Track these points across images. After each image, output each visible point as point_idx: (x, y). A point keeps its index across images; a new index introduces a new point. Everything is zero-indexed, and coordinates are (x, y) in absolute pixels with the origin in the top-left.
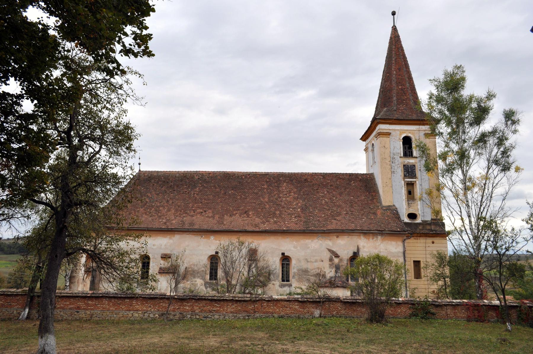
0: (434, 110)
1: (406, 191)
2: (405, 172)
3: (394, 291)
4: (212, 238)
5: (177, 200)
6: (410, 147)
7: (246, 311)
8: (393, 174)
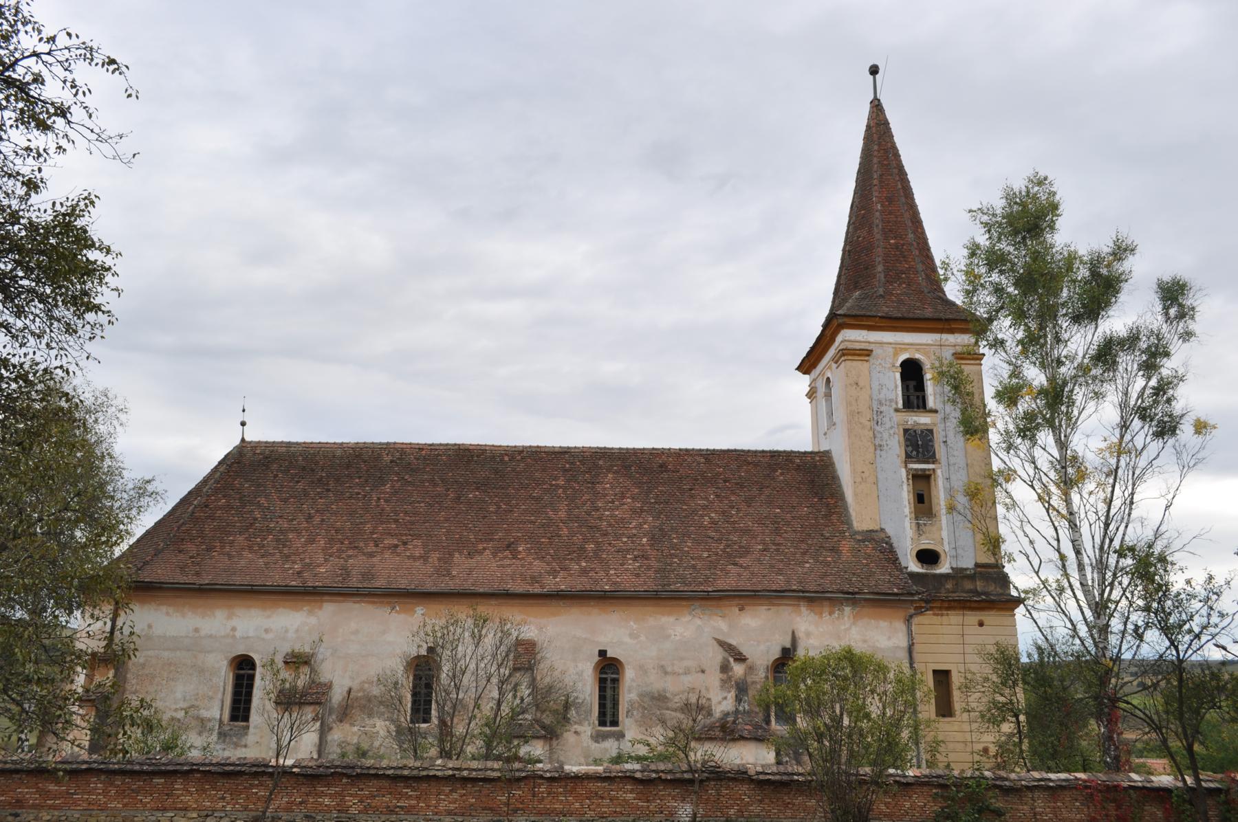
0: (982, 285)
1: (911, 496)
2: (907, 446)
3: (891, 750)
5: (335, 514)
6: (920, 387)
7: (491, 809)
8: (878, 452)
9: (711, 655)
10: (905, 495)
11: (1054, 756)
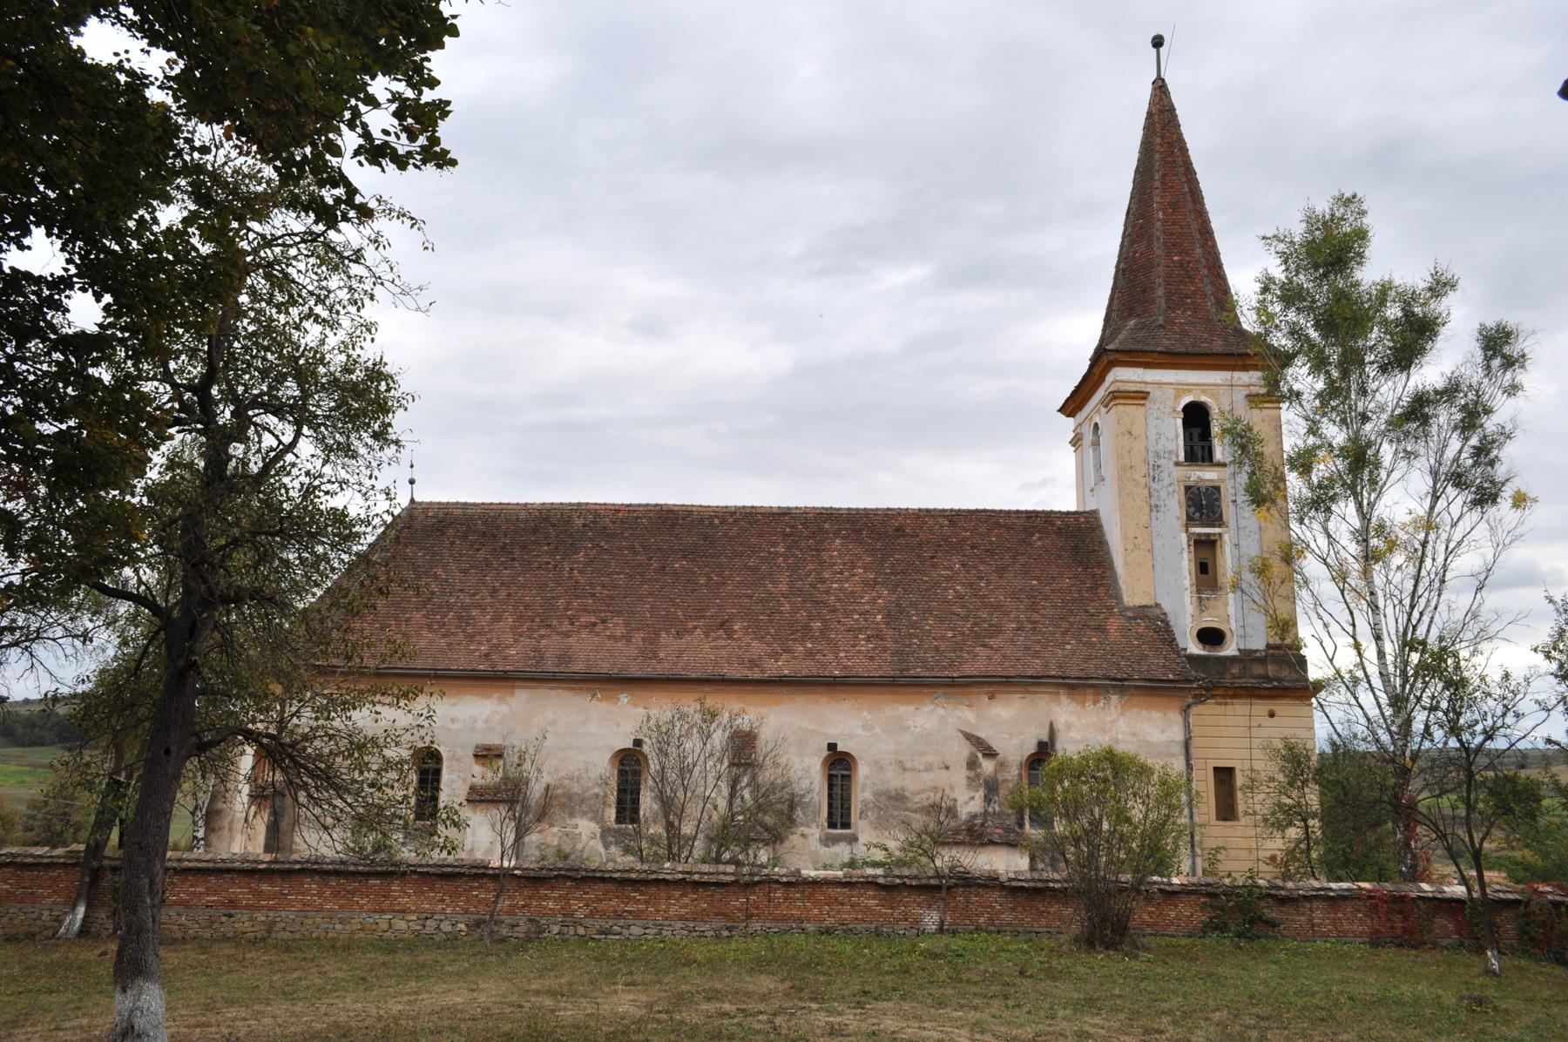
2: (1189, 506)
3: (1157, 857)
4: (624, 699)
5: (524, 586)
6: (1206, 435)
7: (723, 914)
8: (1154, 513)
9: (956, 749)
10: (1186, 564)
11: (1347, 863)
